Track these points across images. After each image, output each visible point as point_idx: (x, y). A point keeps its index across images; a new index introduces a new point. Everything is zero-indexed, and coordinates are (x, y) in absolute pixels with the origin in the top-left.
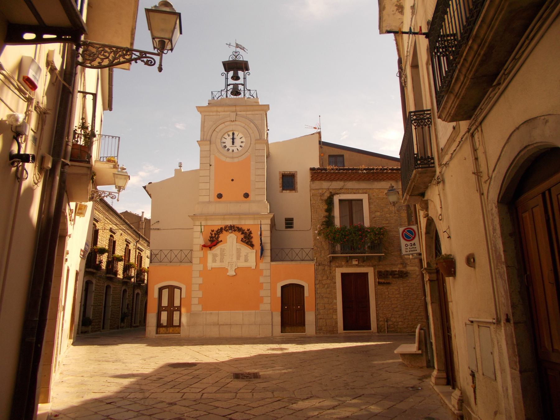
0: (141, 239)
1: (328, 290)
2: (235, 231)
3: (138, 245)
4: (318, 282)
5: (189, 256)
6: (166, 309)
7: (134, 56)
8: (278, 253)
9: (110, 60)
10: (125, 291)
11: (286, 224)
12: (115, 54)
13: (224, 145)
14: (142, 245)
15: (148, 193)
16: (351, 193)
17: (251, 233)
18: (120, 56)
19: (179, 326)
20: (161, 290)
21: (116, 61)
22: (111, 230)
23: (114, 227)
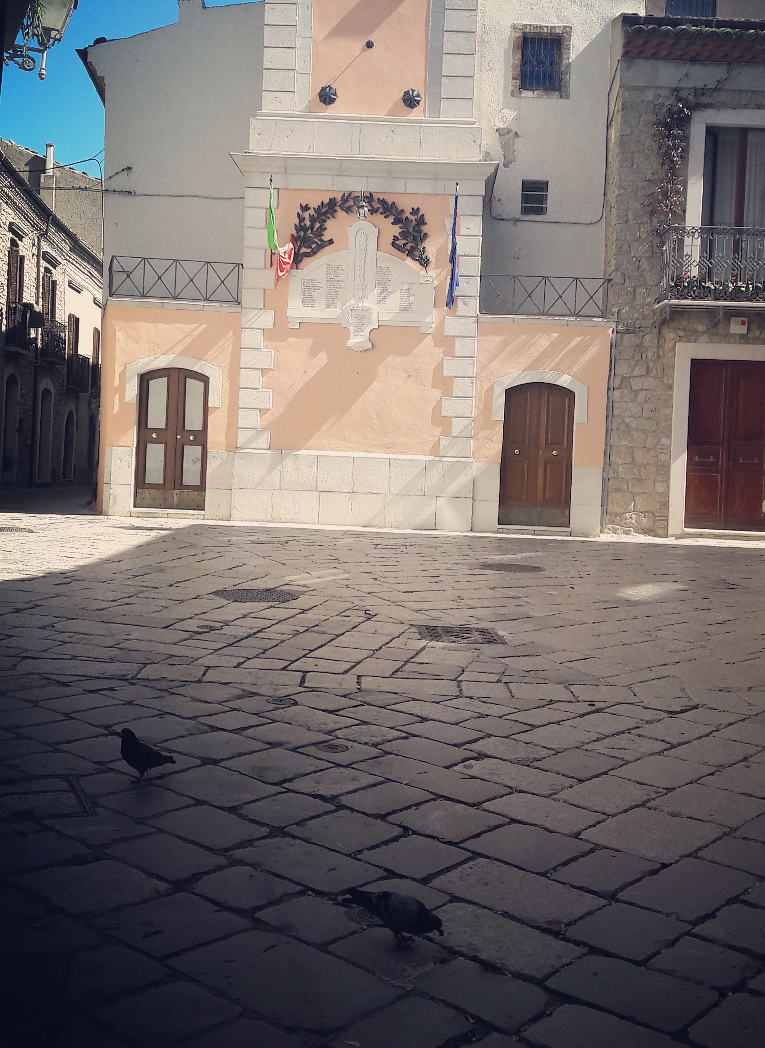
1: (646, 407)
2: (373, 211)
3: (45, 247)
5: (231, 282)
6: (161, 436)
8: (505, 291)
10: (12, 380)
11: (525, 199)
16: (746, 107)
17: (422, 221)
19: (202, 487)
20: (145, 379)
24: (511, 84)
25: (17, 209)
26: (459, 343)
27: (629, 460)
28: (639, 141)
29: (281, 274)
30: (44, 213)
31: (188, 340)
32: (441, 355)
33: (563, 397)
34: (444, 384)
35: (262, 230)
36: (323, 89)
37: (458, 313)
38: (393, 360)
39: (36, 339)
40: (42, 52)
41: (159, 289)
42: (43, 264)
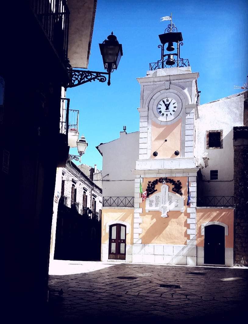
0: (95, 188)
3: (93, 192)
4: (237, 224)
5: (131, 202)
6: (115, 241)
7: (93, 76)
9: (78, 81)
12: (82, 76)
13: (160, 110)
14: (96, 192)
15: (100, 152)
17: (180, 184)
18: (85, 77)
19: (125, 254)
20: (111, 227)
21: (82, 81)
22: (73, 181)
23: (76, 179)
24: (206, 146)
25: (85, 183)
26: (191, 215)
27: (241, 245)
28: (240, 160)
29: (143, 199)
30: (93, 184)
31: (121, 217)
32: (186, 218)
33: (222, 229)
34: (187, 226)
35: (139, 188)
36: (154, 152)
37: (191, 207)
38: (172, 220)
39: (91, 216)
40: (80, 156)
41: (114, 204)
42: (93, 197)
